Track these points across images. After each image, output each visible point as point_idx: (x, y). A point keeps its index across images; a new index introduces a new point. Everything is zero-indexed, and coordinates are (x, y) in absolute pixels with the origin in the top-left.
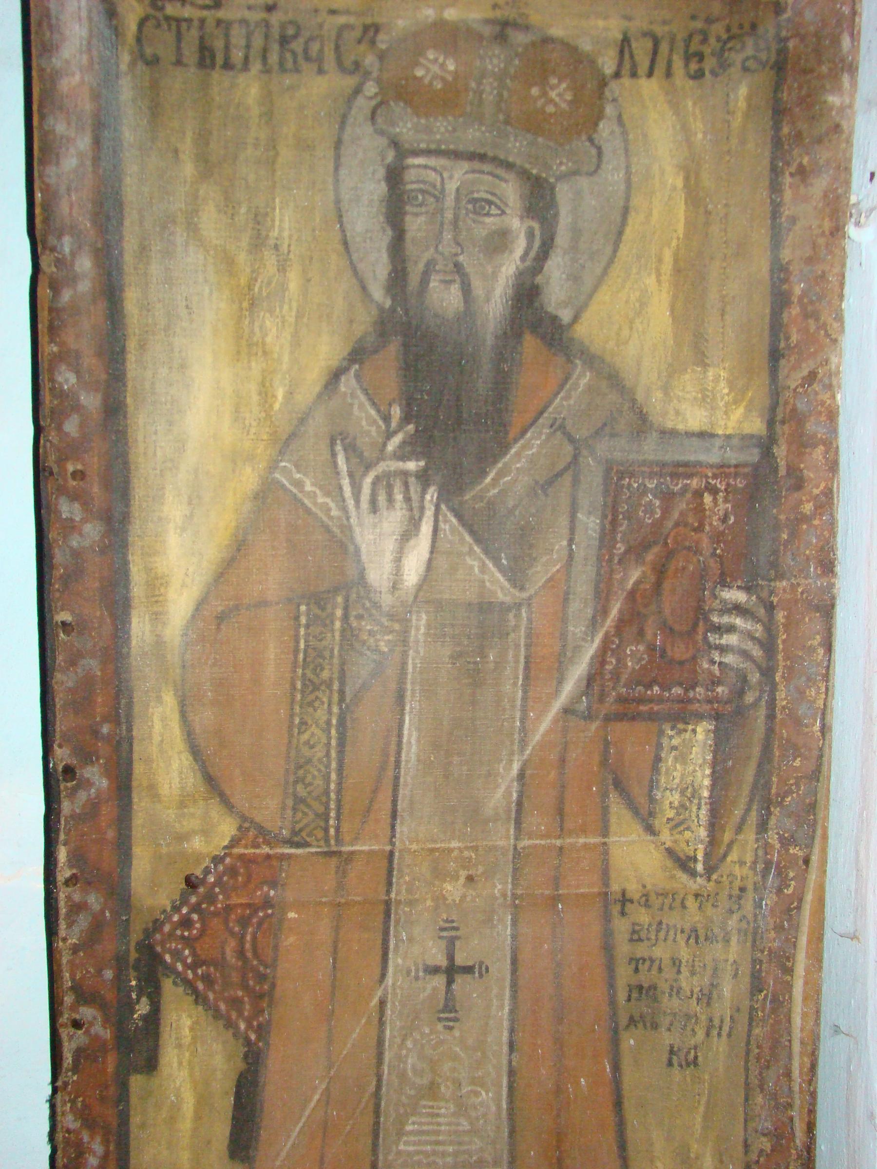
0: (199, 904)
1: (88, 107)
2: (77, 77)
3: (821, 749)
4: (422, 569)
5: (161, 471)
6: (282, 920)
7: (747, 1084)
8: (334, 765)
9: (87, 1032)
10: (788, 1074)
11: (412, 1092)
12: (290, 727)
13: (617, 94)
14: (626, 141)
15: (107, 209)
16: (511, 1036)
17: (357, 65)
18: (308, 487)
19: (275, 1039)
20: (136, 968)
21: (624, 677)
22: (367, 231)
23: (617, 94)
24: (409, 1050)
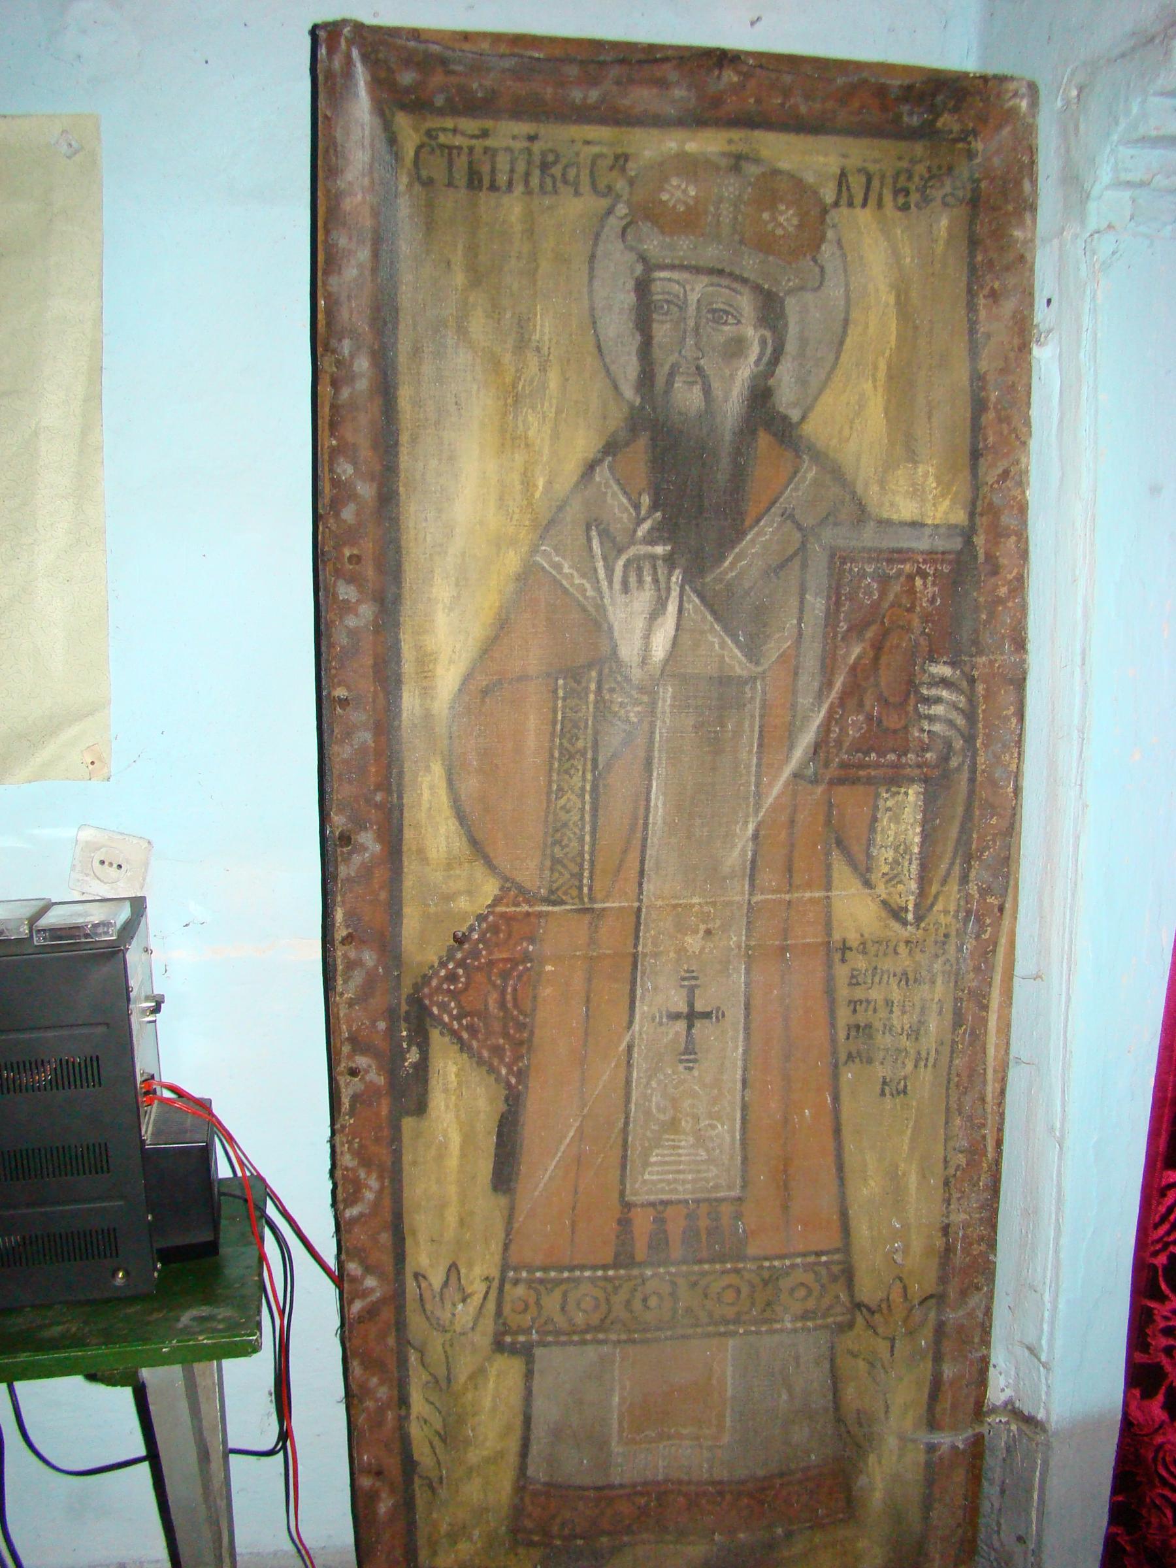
0: (464, 959)
1: (368, 223)
2: (359, 197)
3: (1014, 808)
4: (668, 646)
5: (431, 555)
6: (540, 974)
7: (948, 1110)
8: (588, 828)
9: (362, 1079)
10: (983, 1100)
11: (656, 1128)
12: (549, 794)
13: (836, 220)
14: (845, 262)
15: (384, 315)
16: (744, 1074)
17: (610, 188)
18: (566, 570)
19: (534, 1083)
20: (406, 1020)
21: (846, 744)
22: (618, 336)
23: (836, 220)
24: (653, 1089)
